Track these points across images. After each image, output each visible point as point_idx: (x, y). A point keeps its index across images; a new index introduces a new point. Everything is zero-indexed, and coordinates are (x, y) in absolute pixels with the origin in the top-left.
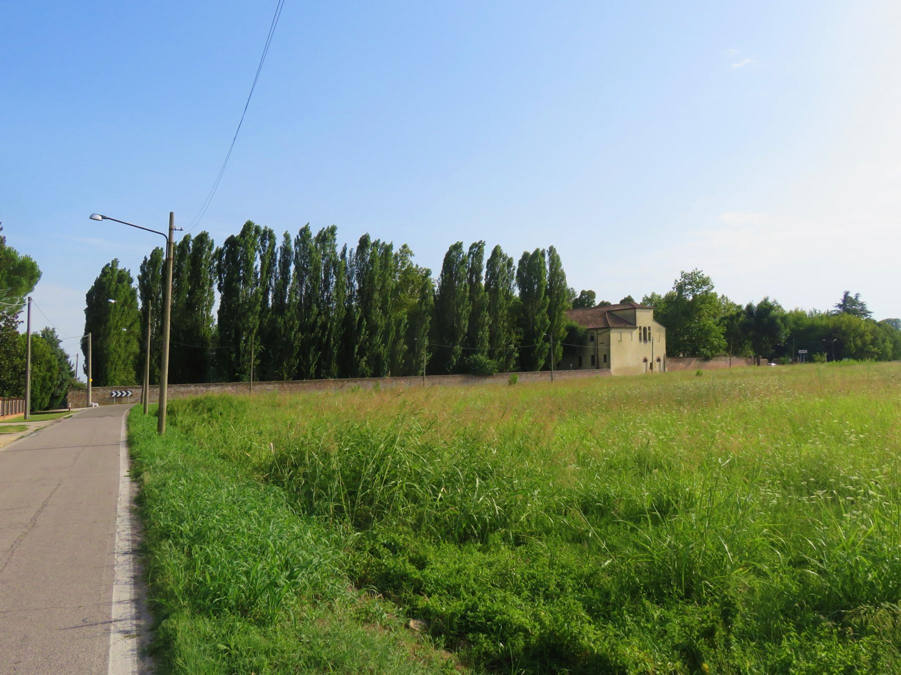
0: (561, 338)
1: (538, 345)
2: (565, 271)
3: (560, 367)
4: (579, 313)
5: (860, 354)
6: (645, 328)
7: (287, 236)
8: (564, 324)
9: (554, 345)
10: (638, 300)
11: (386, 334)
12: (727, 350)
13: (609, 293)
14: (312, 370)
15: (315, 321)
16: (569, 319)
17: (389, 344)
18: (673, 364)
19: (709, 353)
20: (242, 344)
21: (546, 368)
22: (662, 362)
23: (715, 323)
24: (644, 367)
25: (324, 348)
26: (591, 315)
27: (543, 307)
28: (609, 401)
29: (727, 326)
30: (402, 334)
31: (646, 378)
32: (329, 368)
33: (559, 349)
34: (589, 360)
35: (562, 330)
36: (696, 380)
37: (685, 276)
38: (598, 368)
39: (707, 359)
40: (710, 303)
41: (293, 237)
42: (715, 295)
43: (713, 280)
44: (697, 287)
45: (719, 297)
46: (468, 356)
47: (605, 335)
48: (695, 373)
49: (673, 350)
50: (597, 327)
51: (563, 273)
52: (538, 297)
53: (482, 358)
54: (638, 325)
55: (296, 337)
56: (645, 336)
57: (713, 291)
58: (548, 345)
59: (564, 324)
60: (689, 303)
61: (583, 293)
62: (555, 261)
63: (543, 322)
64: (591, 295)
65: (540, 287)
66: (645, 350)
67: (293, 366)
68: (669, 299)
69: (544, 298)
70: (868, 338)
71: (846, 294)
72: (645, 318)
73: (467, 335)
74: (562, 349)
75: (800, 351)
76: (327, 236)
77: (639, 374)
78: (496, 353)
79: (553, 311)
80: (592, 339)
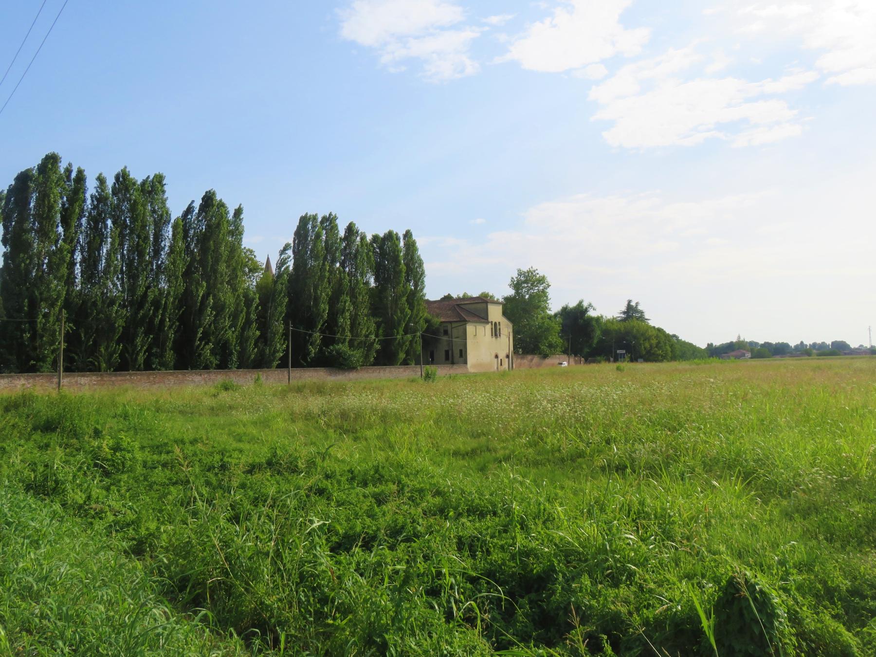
2: (422, 257)
5: (650, 356)
7: (101, 180)
11: (235, 316)
14: (141, 358)
15: (145, 295)
17: (239, 329)
18: (519, 361)
20: (40, 319)
25: (154, 330)
30: (253, 317)
32: (162, 356)
34: (442, 355)
35: (421, 321)
37: (520, 273)
38: (453, 363)
41: (110, 182)
46: (327, 347)
51: (421, 260)
53: (343, 348)
54: (490, 320)
55: (120, 317)
56: (496, 332)
62: (411, 246)
67: (115, 352)
70: (654, 342)
71: (630, 302)
72: (495, 313)
73: (326, 322)
75: (618, 351)
76: (154, 188)
78: (356, 343)
80: (446, 332)
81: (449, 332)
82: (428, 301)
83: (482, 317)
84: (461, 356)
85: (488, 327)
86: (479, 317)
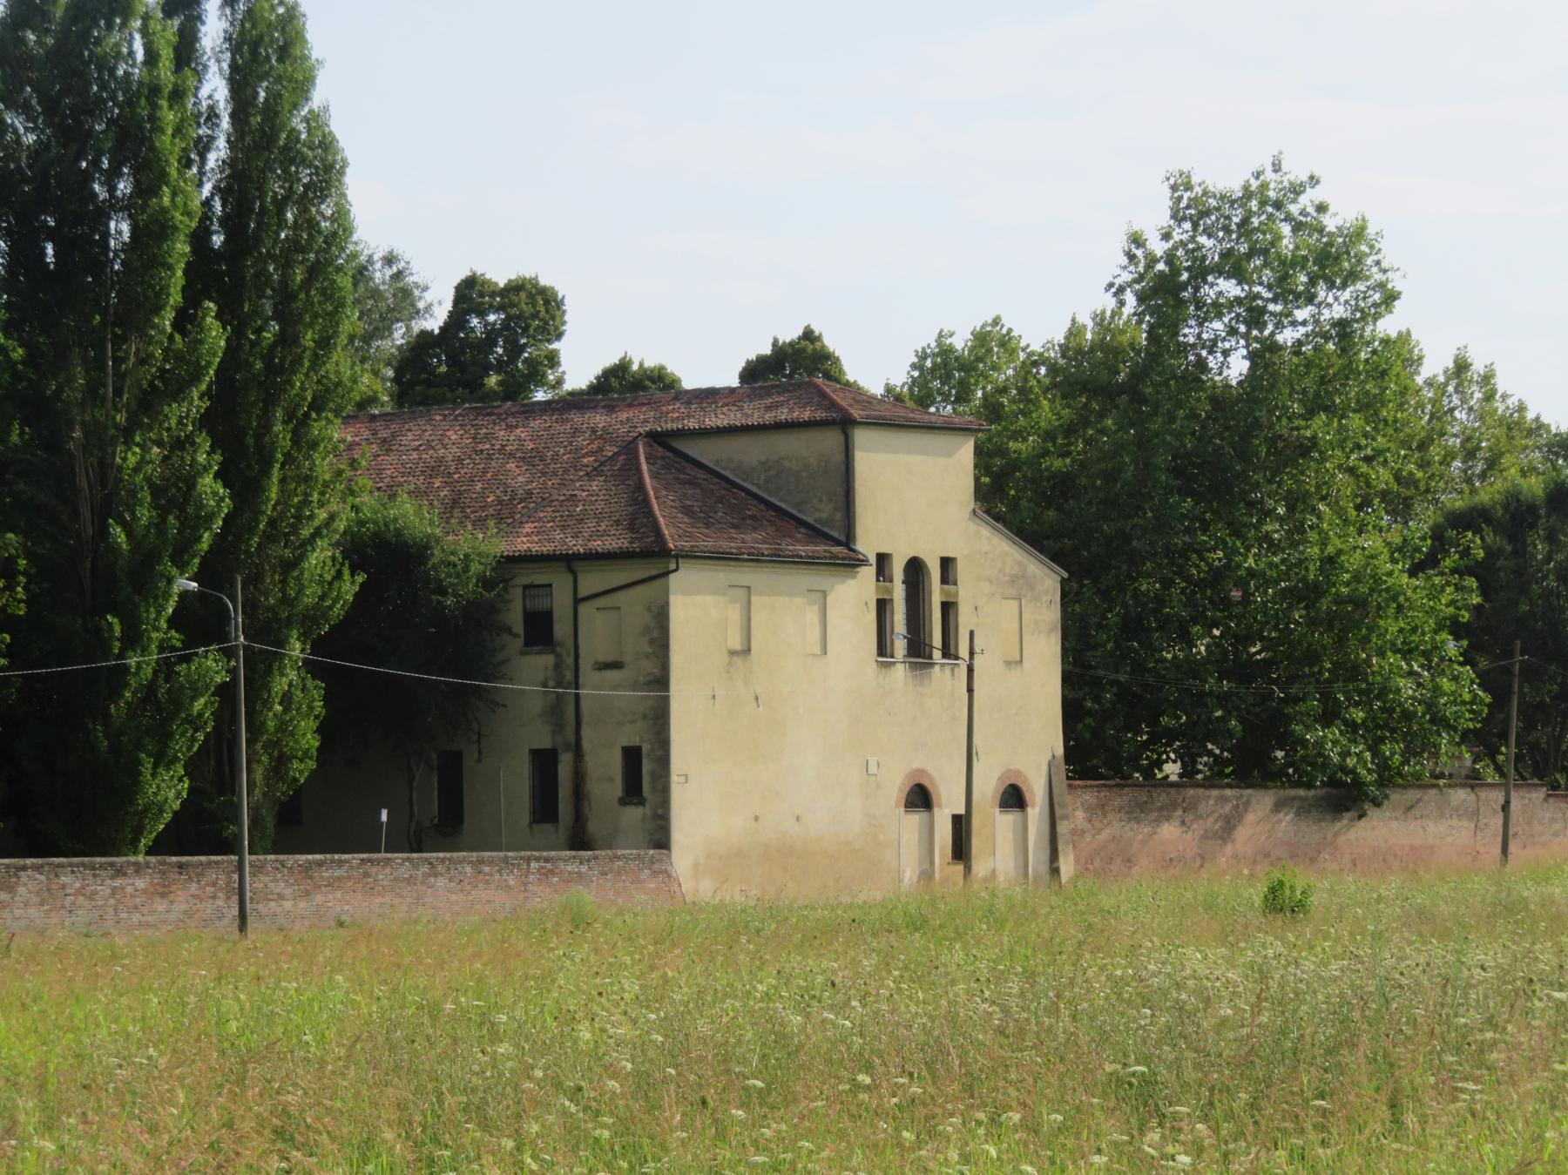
0: (310, 619)
1: (142, 664)
2: (339, 127)
3: (311, 823)
4: (445, 436)
6: (915, 568)
8: (335, 513)
9: (260, 668)
10: (875, 363)
12: (1485, 740)
13: (656, 306)
16: (368, 477)
18: (1114, 828)
19: (1359, 760)
21: (199, 833)
22: (1036, 812)
23: (1400, 550)
24: (908, 845)
26: (528, 459)
27: (177, 390)
28: (644, 1086)
29: (1483, 572)
31: (918, 923)
33: (296, 699)
35: (320, 557)
36: (1271, 945)
37: (1193, 208)
38: (580, 841)
39: (1346, 797)
40: (1368, 406)
42: (1401, 351)
43: (1391, 252)
44: (1283, 290)
45: (1435, 365)
47: (633, 604)
48: (1256, 894)
49: (1117, 730)
50: (577, 546)
51: (327, 144)
52: (136, 310)
54: (868, 543)
56: (919, 622)
57: (1388, 326)
58: (212, 666)
59: (335, 513)
60: (1222, 400)
61: (470, 294)
63: (175, 493)
64: (529, 312)
65: (152, 233)
66: (916, 720)
68: (1093, 376)
69: (186, 320)
74: (315, 697)
77: (872, 893)
79: (251, 416)
80: (539, 630)
81: (561, 629)
82: (687, 392)
83: (805, 525)
84: (633, 791)
85: (853, 596)
86: (786, 520)
